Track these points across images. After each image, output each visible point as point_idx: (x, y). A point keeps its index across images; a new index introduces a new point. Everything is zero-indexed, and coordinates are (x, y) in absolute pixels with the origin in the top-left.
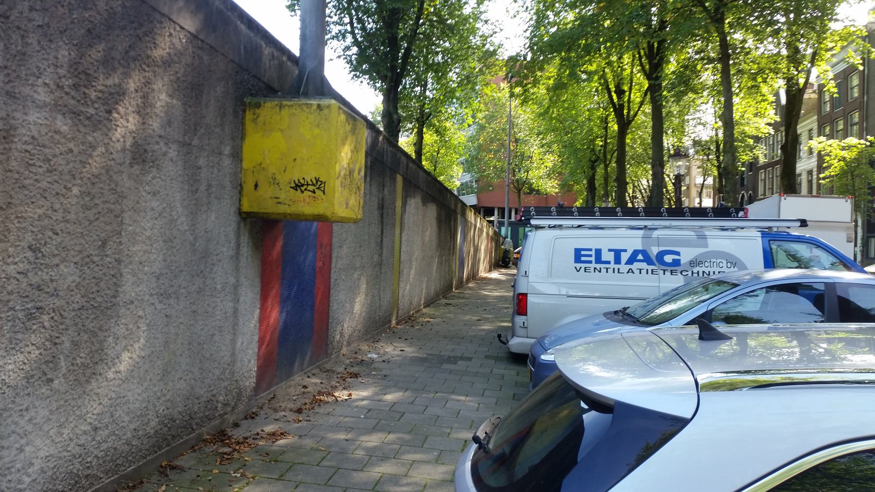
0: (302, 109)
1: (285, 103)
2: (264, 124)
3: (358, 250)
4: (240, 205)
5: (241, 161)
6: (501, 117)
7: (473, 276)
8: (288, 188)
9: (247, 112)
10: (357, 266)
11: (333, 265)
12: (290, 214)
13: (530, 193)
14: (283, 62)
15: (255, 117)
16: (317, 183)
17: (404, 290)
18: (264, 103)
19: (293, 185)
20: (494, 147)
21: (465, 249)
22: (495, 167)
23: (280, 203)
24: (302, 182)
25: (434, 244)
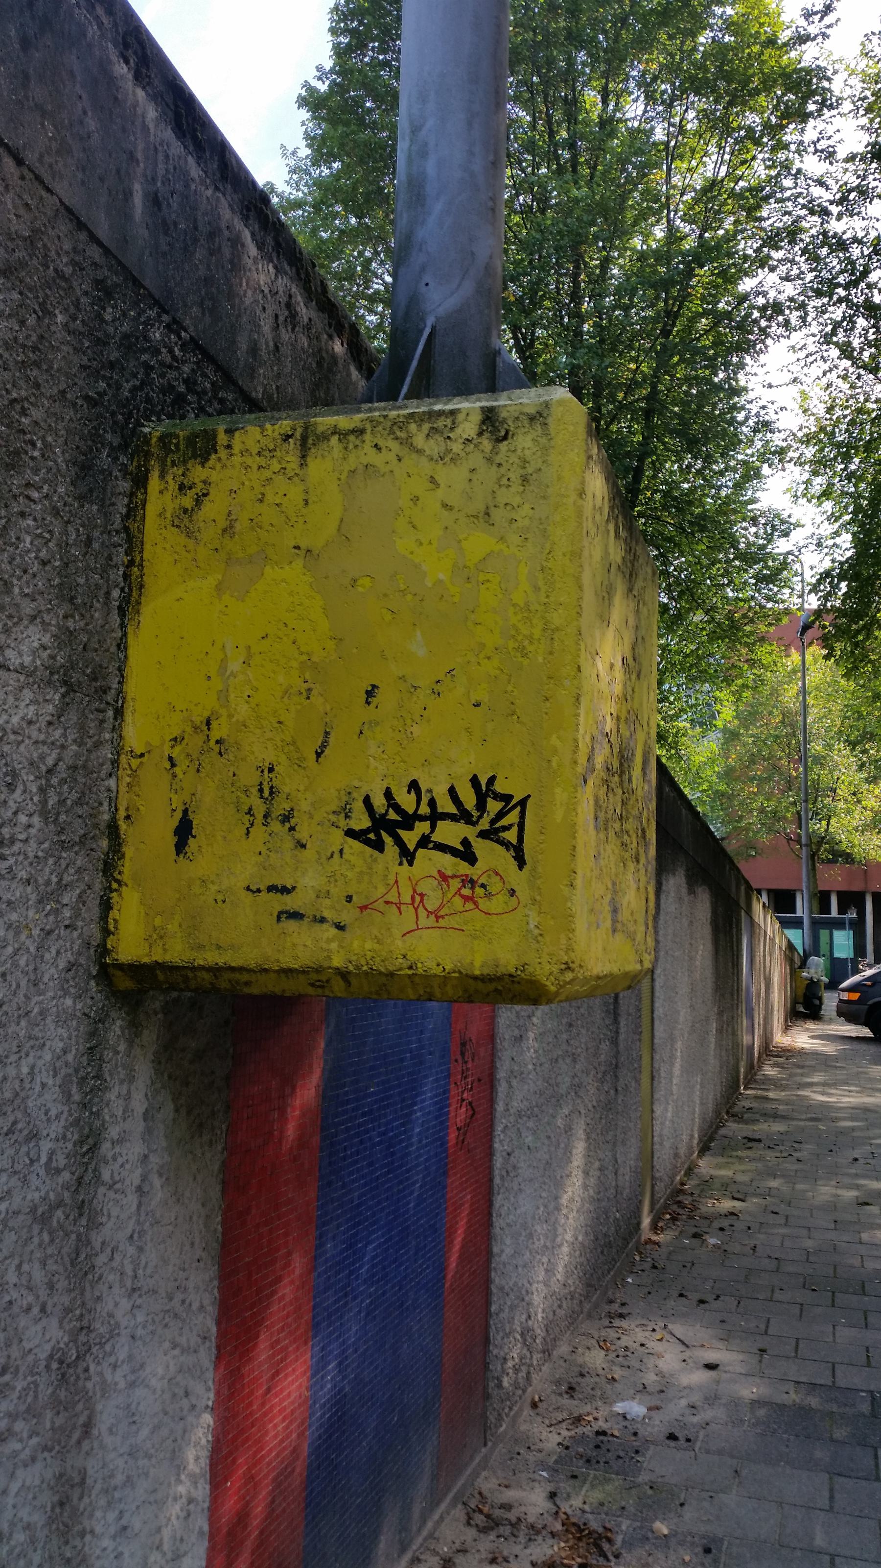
0: (407, 442)
1: (325, 421)
2: (228, 530)
3: (565, 1036)
4: (106, 932)
5: (119, 713)
6: (771, 713)
7: (768, 1050)
8: (337, 838)
9: (154, 483)
10: (563, 1089)
11: (500, 1107)
12: (344, 975)
13: (833, 861)
14: (334, 357)
15: (188, 501)
16: (481, 806)
17: (662, 1124)
18: (230, 432)
19: (361, 821)
20: (758, 770)
21: (754, 989)
22: (762, 810)
23: (296, 916)
24: (407, 802)
25: (710, 984)
